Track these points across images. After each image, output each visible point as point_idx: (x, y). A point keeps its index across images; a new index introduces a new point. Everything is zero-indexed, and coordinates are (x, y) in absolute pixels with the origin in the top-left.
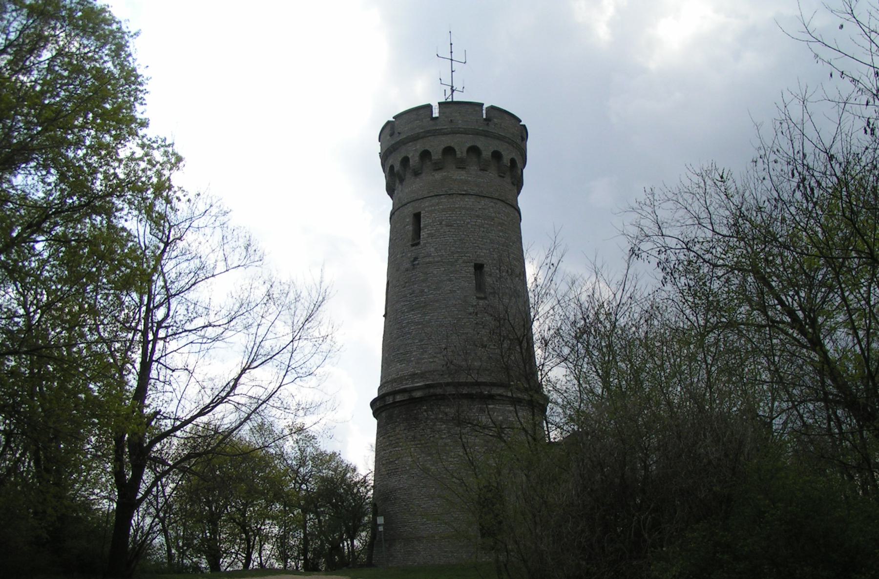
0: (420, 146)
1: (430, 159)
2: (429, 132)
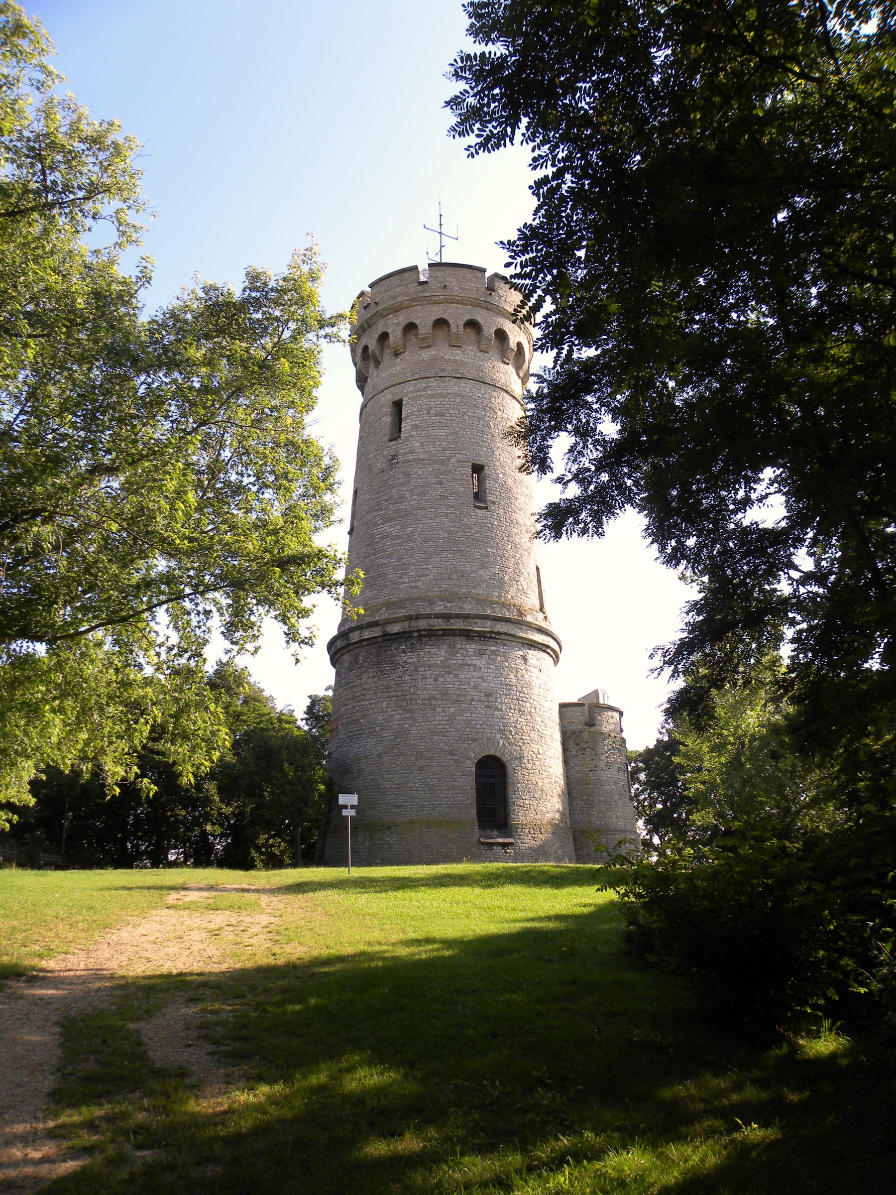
0: (402, 319)
1: (417, 335)
2: (414, 300)
